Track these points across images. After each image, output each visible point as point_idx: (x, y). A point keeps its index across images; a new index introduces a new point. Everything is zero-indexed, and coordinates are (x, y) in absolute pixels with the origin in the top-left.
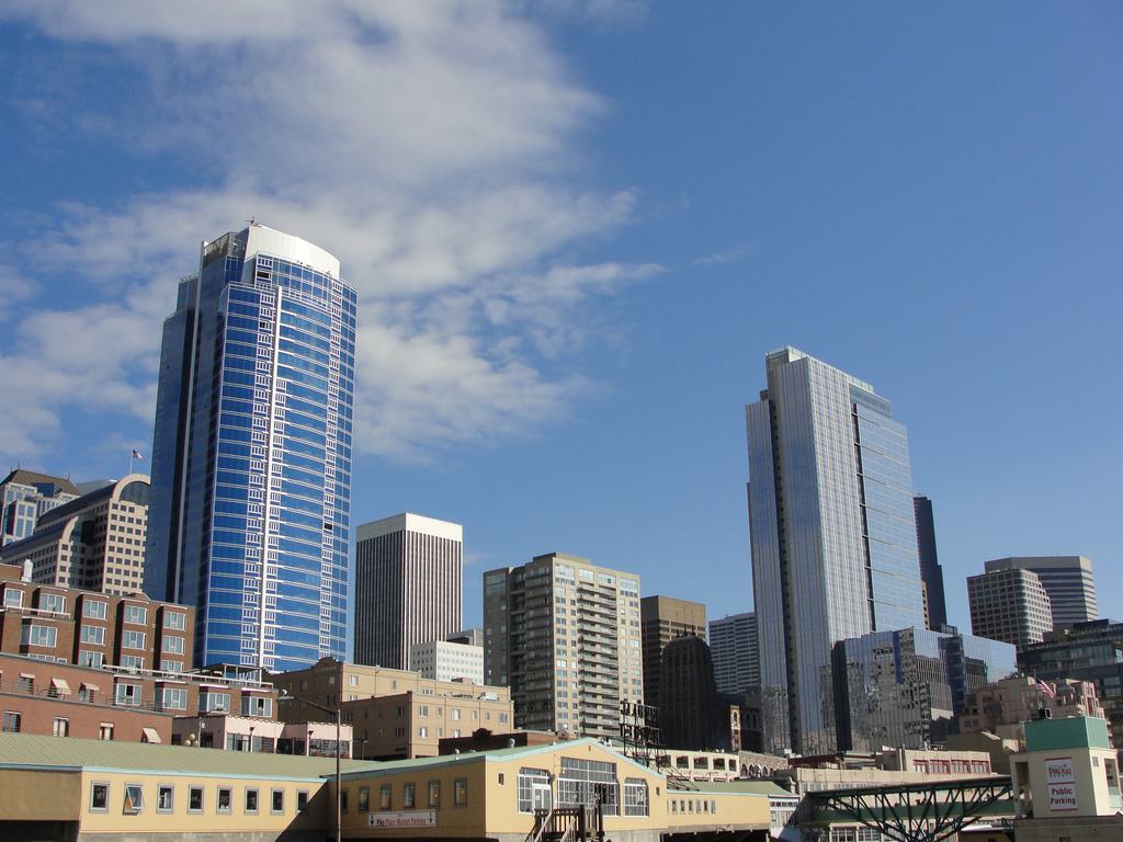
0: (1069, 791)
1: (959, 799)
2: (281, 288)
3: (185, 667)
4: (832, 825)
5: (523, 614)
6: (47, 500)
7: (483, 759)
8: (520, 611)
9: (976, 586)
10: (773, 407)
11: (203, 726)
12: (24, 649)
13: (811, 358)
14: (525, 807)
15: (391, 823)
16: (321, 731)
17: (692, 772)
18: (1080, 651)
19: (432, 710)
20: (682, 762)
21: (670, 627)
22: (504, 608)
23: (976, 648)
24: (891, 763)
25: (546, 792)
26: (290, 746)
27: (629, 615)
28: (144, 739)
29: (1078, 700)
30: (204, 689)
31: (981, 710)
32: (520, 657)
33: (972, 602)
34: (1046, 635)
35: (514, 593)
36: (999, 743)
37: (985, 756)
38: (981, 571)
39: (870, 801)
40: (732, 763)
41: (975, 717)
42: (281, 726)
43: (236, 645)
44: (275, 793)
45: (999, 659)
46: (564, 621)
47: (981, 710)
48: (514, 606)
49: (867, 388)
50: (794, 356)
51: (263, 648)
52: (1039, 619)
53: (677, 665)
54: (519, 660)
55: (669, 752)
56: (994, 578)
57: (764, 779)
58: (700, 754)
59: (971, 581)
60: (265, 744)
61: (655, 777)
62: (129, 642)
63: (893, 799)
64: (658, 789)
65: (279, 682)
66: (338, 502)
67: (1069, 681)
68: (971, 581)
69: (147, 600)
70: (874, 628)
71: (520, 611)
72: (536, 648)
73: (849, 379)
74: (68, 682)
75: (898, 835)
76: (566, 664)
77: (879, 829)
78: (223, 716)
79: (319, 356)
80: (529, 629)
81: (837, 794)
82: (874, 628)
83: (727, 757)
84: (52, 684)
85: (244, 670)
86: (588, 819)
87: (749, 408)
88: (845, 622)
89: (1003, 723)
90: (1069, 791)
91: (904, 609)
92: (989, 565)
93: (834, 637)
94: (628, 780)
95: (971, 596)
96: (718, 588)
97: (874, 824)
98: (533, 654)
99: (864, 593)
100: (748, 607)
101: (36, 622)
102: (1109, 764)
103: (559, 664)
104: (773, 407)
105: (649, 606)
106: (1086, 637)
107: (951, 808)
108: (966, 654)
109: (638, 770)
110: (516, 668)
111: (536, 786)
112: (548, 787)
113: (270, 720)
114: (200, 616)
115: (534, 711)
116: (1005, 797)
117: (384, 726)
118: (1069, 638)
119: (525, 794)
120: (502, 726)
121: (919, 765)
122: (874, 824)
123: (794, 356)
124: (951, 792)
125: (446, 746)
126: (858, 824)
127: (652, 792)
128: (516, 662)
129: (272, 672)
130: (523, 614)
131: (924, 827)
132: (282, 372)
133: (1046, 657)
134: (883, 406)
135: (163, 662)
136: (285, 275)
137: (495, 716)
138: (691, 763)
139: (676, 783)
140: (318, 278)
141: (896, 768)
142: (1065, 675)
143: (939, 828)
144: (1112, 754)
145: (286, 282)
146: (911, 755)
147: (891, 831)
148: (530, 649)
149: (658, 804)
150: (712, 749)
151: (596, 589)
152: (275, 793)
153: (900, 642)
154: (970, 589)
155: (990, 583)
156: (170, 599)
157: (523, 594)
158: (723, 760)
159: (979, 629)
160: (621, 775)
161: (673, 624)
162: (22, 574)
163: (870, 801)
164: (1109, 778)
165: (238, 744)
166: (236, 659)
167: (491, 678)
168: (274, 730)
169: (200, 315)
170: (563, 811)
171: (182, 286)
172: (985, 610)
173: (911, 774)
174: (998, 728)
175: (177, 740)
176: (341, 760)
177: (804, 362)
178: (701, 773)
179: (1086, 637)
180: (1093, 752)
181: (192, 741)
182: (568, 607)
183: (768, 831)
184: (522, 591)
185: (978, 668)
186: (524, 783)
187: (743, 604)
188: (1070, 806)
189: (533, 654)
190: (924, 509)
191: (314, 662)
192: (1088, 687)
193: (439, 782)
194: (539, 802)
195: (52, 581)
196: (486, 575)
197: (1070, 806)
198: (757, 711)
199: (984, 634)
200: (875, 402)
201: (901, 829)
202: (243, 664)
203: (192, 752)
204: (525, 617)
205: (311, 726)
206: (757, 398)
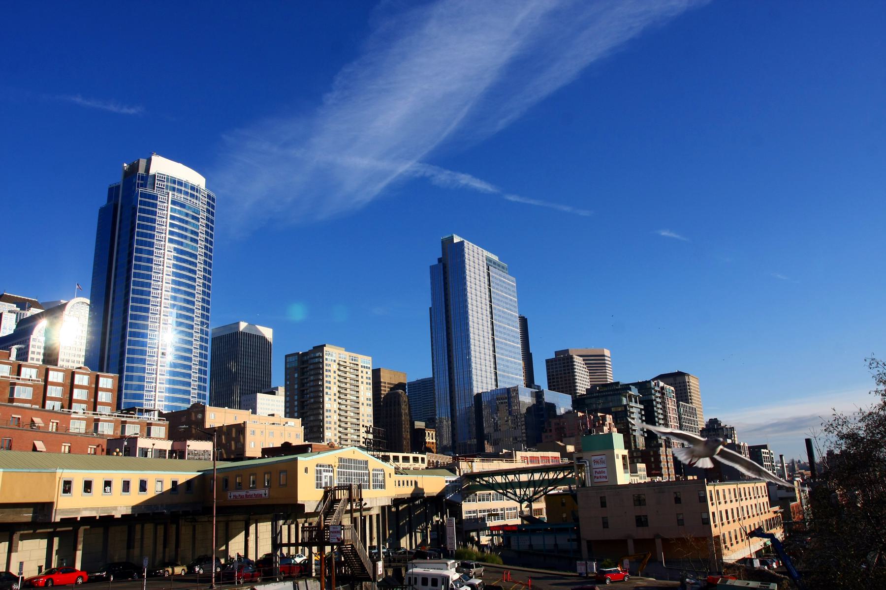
0: (604, 472)
1: (546, 477)
2: (171, 193)
3: (112, 410)
4: (478, 493)
6: (22, 312)
7: (296, 459)
10: (445, 267)
11: (126, 443)
12: (12, 400)
13: (466, 242)
14: (319, 486)
15: (242, 497)
16: (194, 445)
17: (402, 465)
19: (258, 432)
20: (396, 459)
22: (296, 375)
23: (550, 396)
24: (509, 457)
25: (331, 477)
26: (178, 453)
27: (366, 376)
28: (35, 449)
29: (604, 424)
30: (125, 422)
31: (553, 431)
32: (306, 403)
33: (548, 373)
34: (587, 390)
36: (565, 447)
37: (558, 454)
39: (499, 479)
40: (423, 459)
42: (171, 442)
43: (141, 397)
44: (86, 482)
45: (563, 403)
46: (330, 382)
47: (553, 431)
48: (303, 374)
49: (495, 258)
50: (457, 239)
51: (159, 396)
52: (583, 383)
55: (387, 454)
56: (560, 360)
57: (442, 468)
58: (405, 455)
59: (547, 361)
60: (161, 453)
61: (389, 467)
62: (77, 394)
63: (511, 477)
65: (167, 417)
66: (203, 315)
67: (599, 414)
68: (547, 361)
69: (89, 371)
70: (497, 386)
72: (314, 397)
73: (486, 253)
74: (42, 419)
75: (513, 497)
76: (330, 403)
77: (503, 494)
78: (136, 438)
79: (193, 232)
81: (482, 475)
82: (497, 386)
83: (420, 456)
84: (32, 421)
85: (148, 411)
86: (354, 491)
87: (432, 267)
88: (482, 382)
89: (565, 436)
90: (604, 472)
91: (514, 377)
92: (557, 353)
93: (476, 391)
95: (548, 369)
96: (415, 365)
97: (501, 491)
98: (312, 400)
99: (493, 364)
100: (429, 375)
101: (19, 384)
102: (624, 457)
103: (327, 406)
104: (445, 267)
105: (376, 373)
106: (607, 391)
107: (541, 482)
108: (546, 400)
109: (380, 464)
110: (303, 408)
111: (324, 474)
112: (331, 474)
113: (164, 439)
114: (120, 380)
115: (314, 431)
116: (570, 476)
117: (231, 440)
118: (599, 392)
119: (319, 478)
120: (298, 440)
121: (522, 458)
122: (501, 491)
123: (457, 239)
125: (267, 452)
126: (492, 492)
127: (387, 476)
128: (302, 405)
129: (164, 412)
131: (527, 493)
132: (171, 241)
133: (588, 401)
134: (503, 267)
135: (74, 405)
136: (173, 185)
137: (293, 435)
138: (401, 459)
139: (397, 471)
140: (193, 188)
141: (512, 461)
142: (597, 411)
143: (535, 493)
144: (626, 452)
145: (174, 189)
146: (519, 454)
147: (509, 495)
148: (311, 398)
149: (390, 482)
150: (412, 452)
152: (86, 482)
153: (510, 394)
154: (547, 366)
156: (102, 371)
158: (389, 456)
159: (551, 388)
160: (370, 467)
162: (10, 356)
163: (499, 479)
164: (624, 465)
165: (144, 452)
166: (142, 404)
167: (290, 413)
168: (167, 445)
169: (122, 207)
170: (340, 488)
171: (111, 190)
173: (518, 464)
174: (564, 439)
175: (109, 452)
176: (805, 459)
177: (462, 243)
178: (406, 465)
179: (607, 391)
180: (616, 452)
181: (118, 453)
185: (552, 407)
186: (319, 472)
187: (424, 371)
188: (605, 480)
189: (312, 400)
190: (524, 322)
191: (189, 406)
192: (609, 418)
193: (286, 471)
194: (326, 483)
195: (26, 360)
196: (286, 356)
197: (605, 480)
199: (554, 390)
200: (499, 265)
201: (515, 494)
202: (145, 407)
203: (118, 457)
205: (188, 442)
206: (436, 262)
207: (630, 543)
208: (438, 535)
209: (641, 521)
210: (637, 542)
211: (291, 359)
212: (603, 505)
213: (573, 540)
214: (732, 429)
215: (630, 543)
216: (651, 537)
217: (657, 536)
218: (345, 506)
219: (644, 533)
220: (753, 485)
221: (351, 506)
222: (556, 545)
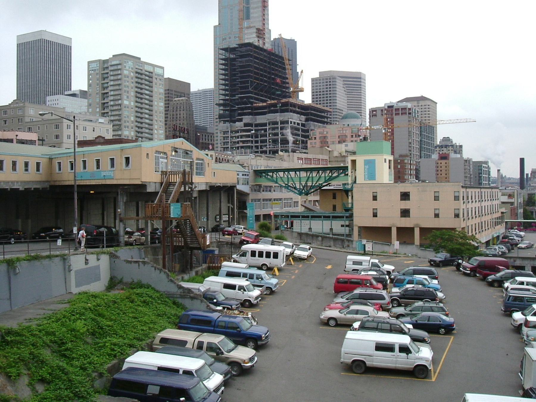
5: (107, 83)
8: (106, 81)
9: (315, 82)
18: (263, 131)
21: (173, 93)
35: (103, 82)
38: (317, 76)
40: (211, 156)
41: (315, 141)
47: (318, 138)
53: (177, 111)
54: (106, 105)
59: (313, 80)
64: (112, 160)
68: (313, 80)
71: (106, 81)
80: (111, 101)
94: (198, 159)
111: (161, 160)
112: (166, 161)
119: (157, 164)
124: (295, 173)
130: (107, 83)
151: (143, 72)
154: (312, 84)
155: (318, 82)
157: (108, 73)
161: (175, 91)
172: (318, 93)
182: (129, 79)
183: (235, 186)
184: (107, 72)
186: (157, 158)
196: (89, 63)
198: (213, 134)
204: (109, 75)
207: (417, 232)
208: (229, 218)
209: (405, 213)
210: (399, 229)
211: (94, 65)
212: (375, 198)
213: (347, 226)
214: (461, 146)
215: (417, 232)
216: (412, 226)
217: (417, 225)
218: (180, 187)
219: (405, 223)
220: (479, 190)
221: (185, 188)
222: (331, 229)
